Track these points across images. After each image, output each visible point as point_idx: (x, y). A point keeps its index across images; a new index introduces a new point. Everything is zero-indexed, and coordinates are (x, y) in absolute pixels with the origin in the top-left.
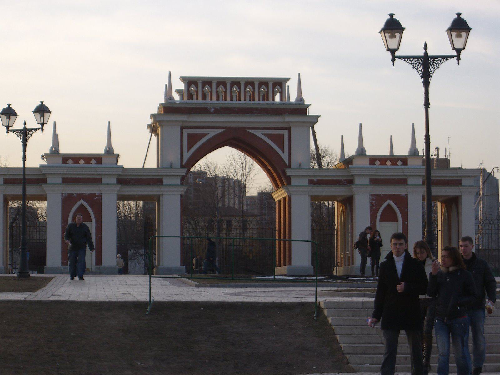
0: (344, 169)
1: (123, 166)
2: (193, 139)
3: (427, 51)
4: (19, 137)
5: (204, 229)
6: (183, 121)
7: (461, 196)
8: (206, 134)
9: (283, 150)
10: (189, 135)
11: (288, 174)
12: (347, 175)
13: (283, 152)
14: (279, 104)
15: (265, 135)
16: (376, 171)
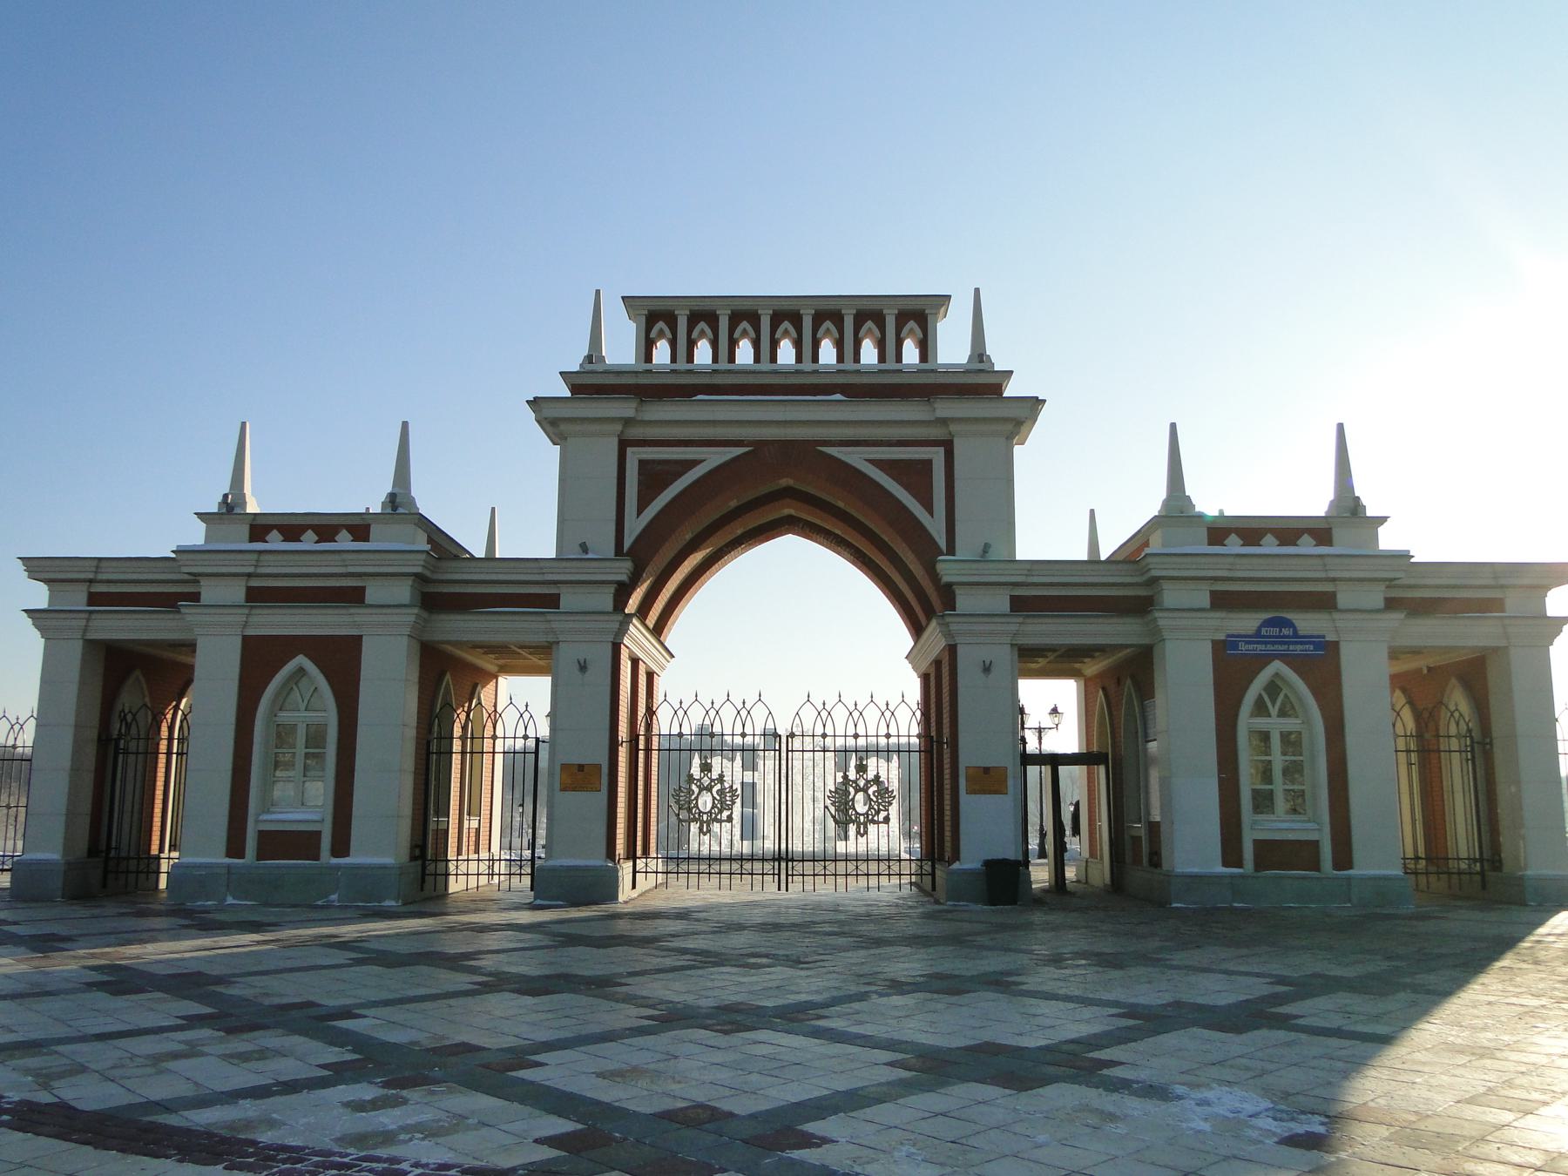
6: (628, 422)
8: (694, 463)
10: (927, 464)
11: (946, 579)
13: (932, 514)
14: (919, 371)
15: (878, 463)
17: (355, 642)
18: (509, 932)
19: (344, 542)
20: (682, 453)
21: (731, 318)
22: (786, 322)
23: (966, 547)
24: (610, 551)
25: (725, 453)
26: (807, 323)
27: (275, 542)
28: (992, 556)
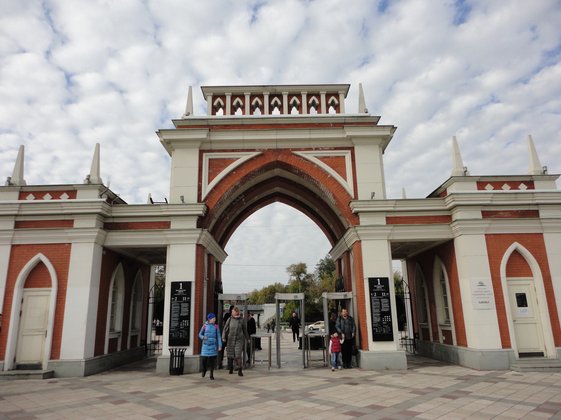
0: (324, 324)
6: (203, 141)
8: (232, 161)
9: (345, 178)
13: (346, 179)
18: (535, 373)
21: (269, 97)
24: (195, 200)
27: (30, 199)
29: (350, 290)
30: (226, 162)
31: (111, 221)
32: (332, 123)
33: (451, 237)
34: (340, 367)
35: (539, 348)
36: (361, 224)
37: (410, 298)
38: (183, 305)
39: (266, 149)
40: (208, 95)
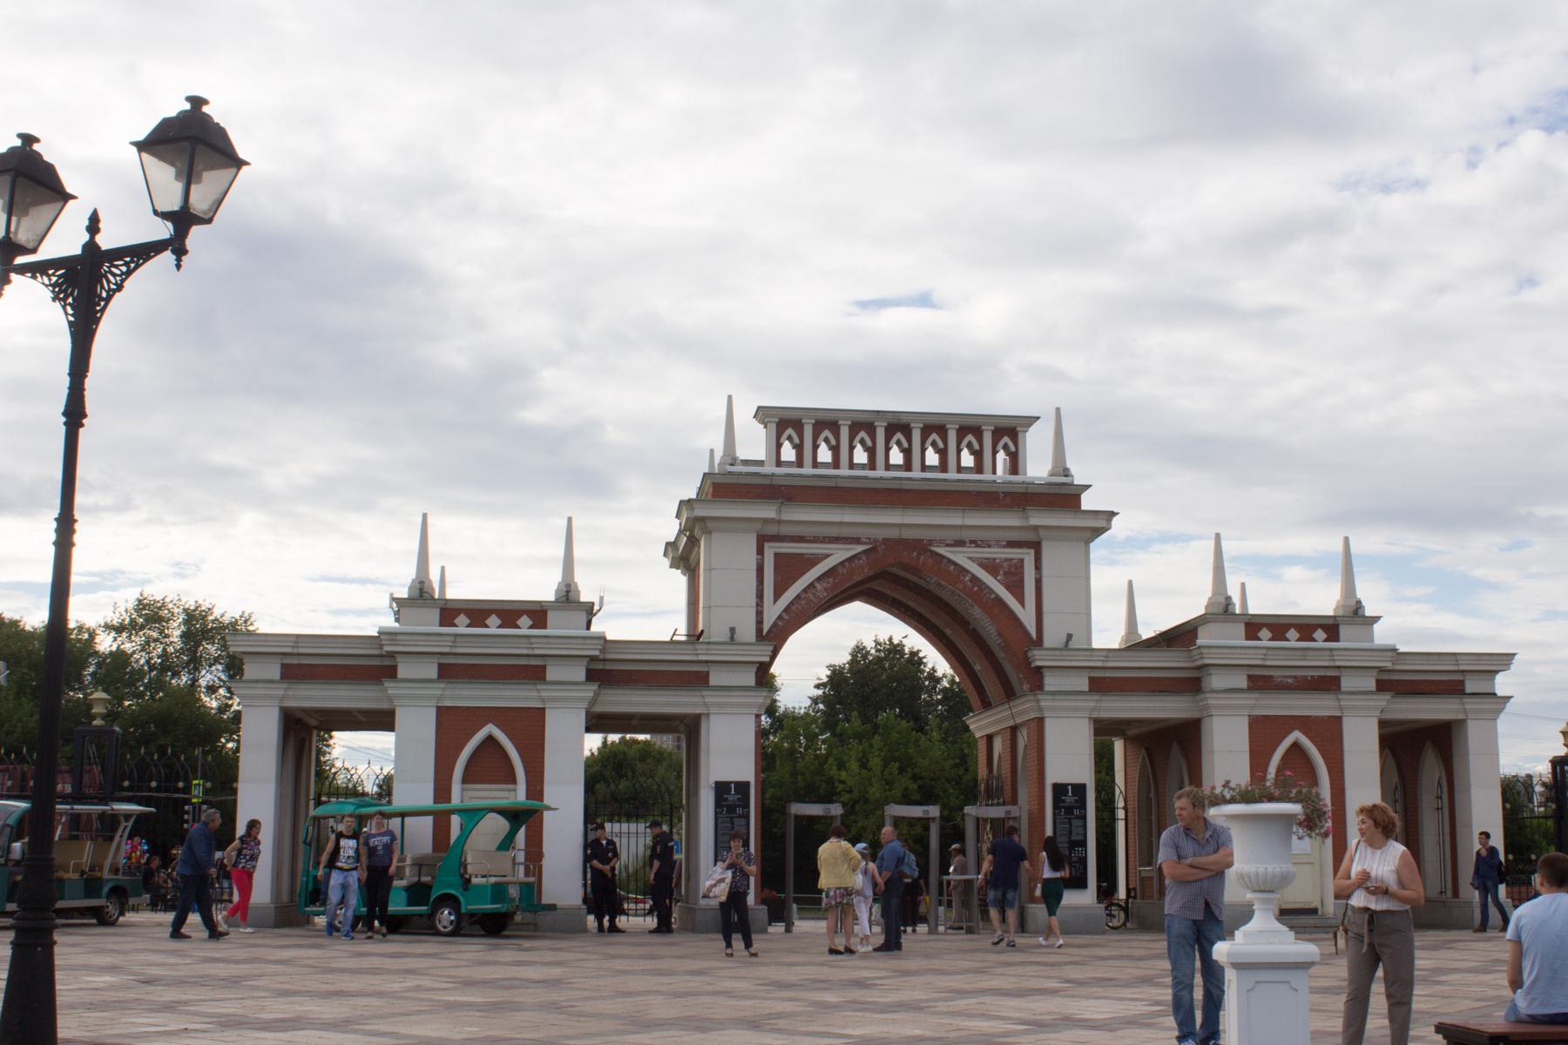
1: (604, 633)
2: (789, 569)
3: (99, 239)
4: (60, 300)
5: (123, 644)
6: (766, 521)
7: (1461, 723)
8: (813, 561)
9: (1022, 603)
12: (1190, 665)
13: (1023, 606)
16: (1265, 655)
17: (540, 713)
19: (524, 626)
20: (781, 547)
21: (994, 432)
22: (790, 429)
23: (1052, 637)
25: (849, 549)
26: (845, 433)
28: (1072, 645)
29: (1014, 801)
30: (812, 561)
31: (599, 666)
32: (1003, 493)
33: (1195, 715)
34: (941, 929)
35: (1312, 903)
36: (1047, 688)
37: (1126, 819)
38: (737, 821)
39: (880, 538)
40: (770, 422)
